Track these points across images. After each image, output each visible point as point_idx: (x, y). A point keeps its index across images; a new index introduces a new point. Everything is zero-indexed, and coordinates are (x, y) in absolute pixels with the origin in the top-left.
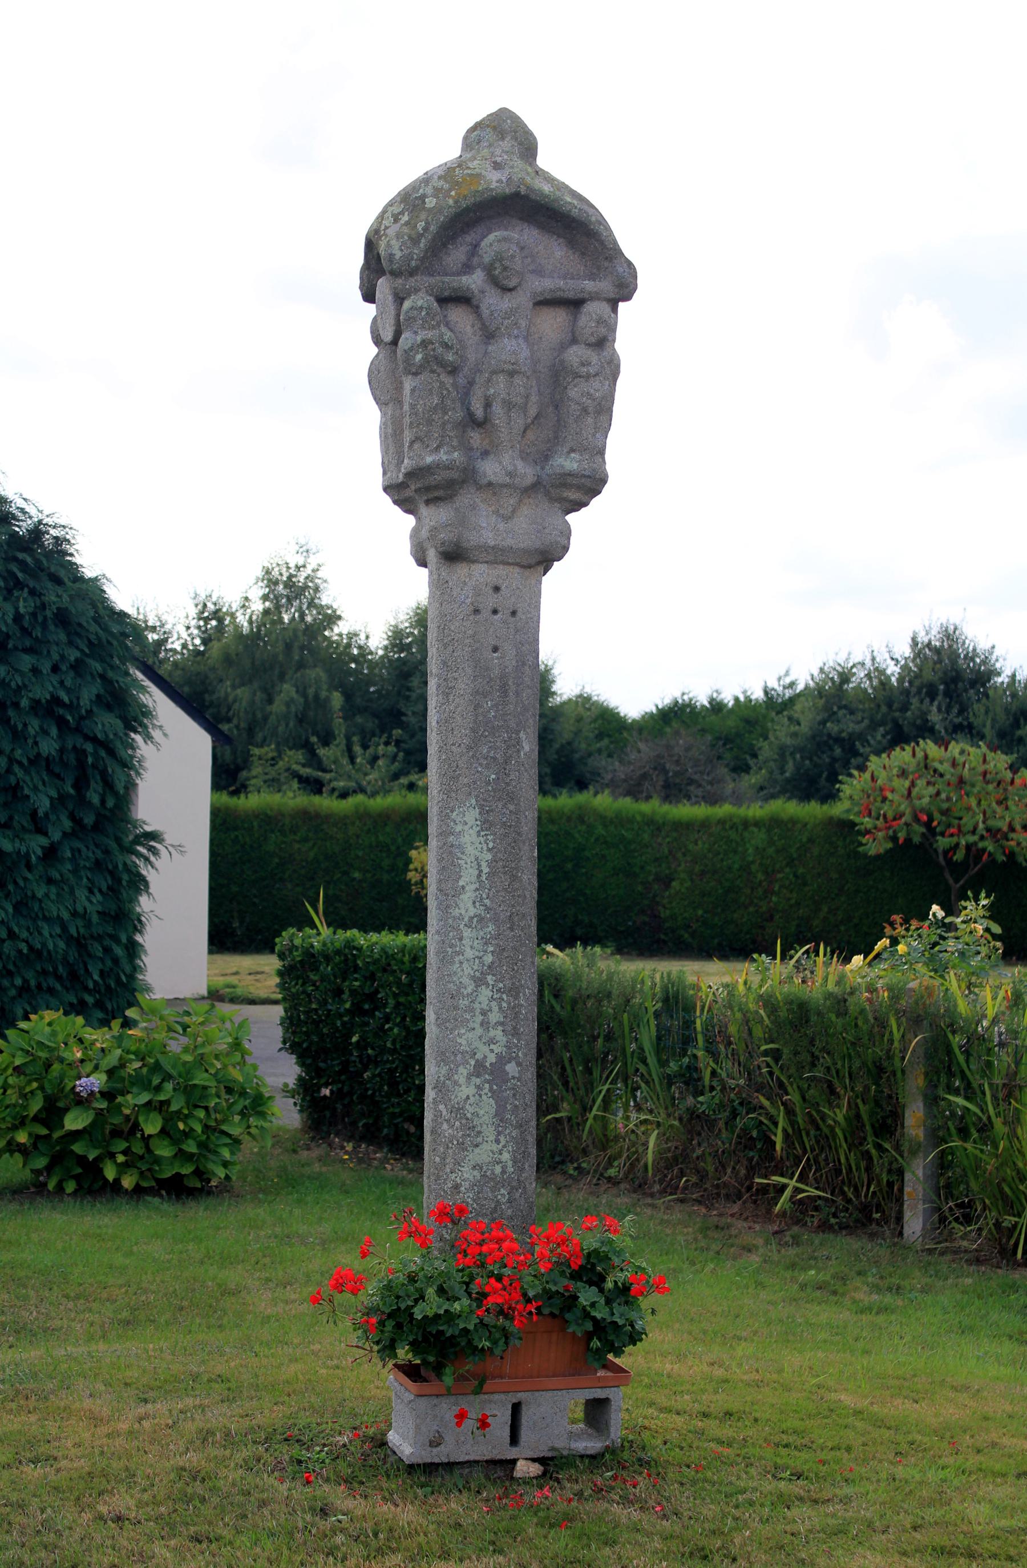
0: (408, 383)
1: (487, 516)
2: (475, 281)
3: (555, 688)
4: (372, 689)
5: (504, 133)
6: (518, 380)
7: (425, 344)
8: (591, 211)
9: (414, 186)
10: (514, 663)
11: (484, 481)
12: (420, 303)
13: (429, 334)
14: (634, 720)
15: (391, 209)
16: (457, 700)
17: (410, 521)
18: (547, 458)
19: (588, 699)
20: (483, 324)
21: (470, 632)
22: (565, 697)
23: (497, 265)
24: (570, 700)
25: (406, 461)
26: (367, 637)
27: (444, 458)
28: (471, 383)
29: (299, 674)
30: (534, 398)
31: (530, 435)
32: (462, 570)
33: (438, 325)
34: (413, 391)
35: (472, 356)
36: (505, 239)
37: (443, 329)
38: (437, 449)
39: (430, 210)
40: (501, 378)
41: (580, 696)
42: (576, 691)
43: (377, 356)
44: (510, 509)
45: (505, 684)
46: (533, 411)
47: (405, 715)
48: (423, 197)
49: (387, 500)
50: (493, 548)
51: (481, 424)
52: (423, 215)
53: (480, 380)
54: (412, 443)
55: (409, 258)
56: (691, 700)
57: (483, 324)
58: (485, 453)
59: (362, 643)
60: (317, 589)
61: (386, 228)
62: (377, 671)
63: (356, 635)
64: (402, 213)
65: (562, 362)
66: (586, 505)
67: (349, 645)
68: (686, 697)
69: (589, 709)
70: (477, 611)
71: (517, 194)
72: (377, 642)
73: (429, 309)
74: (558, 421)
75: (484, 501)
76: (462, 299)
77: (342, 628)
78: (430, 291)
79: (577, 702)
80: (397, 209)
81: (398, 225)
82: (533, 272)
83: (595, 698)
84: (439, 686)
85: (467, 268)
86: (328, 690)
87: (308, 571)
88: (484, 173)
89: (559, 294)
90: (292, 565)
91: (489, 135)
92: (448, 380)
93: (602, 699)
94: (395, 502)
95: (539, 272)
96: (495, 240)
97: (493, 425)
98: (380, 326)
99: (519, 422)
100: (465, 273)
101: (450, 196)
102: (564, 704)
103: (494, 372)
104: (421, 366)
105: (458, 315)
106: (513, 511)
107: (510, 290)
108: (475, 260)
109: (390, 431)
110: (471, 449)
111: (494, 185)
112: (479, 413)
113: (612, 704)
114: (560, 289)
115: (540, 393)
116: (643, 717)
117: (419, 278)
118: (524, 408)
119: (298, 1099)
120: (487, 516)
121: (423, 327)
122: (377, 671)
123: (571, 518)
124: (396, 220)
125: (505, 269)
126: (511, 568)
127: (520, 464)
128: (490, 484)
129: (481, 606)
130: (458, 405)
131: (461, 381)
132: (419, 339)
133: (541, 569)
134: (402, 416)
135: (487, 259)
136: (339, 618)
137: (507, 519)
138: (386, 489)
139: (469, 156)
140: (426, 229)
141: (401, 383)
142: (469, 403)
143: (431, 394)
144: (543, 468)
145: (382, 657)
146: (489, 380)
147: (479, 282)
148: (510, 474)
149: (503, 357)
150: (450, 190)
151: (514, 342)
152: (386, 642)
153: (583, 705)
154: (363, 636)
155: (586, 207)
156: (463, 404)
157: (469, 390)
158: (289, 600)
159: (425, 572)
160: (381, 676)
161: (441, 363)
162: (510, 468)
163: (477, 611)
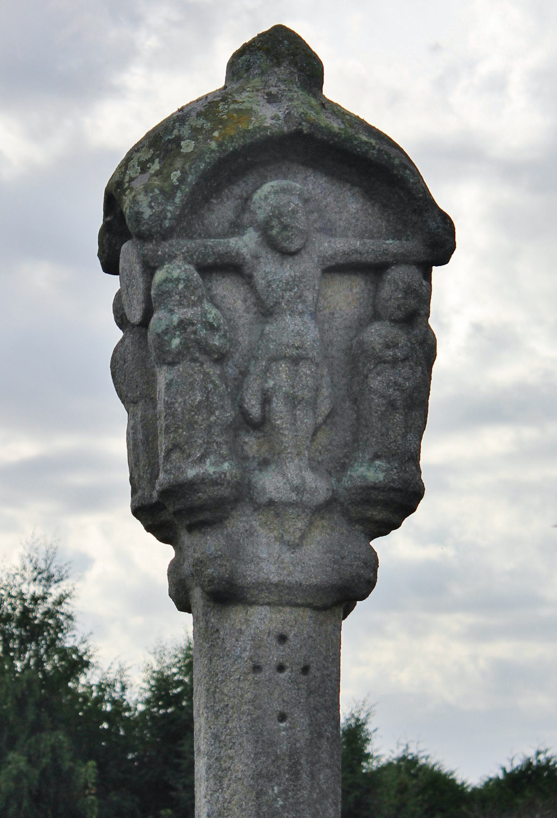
0: (163, 376)
1: (268, 545)
2: (246, 243)
3: (369, 749)
4: (130, 756)
5: (280, 57)
6: (305, 369)
7: (183, 325)
8: (393, 152)
9: (166, 126)
10: (307, 734)
11: (263, 500)
12: (176, 273)
13: (189, 313)
14: (475, 790)
15: (137, 156)
16: (234, 786)
17: (168, 552)
18: (344, 467)
19: (414, 762)
20: (258, 298)
21: (249, 696)
22: (384, 761)
23: (274, 223)
24: (390, 764)
25: (161, 476)
26: (124, 688)
27: (211, 470)
28: (244, 373)
29: (33, 739)
30: (325, 392)
31: (322, 438)
32: (237, 615)
33: (200, 300)
34: (169, 385)
35: (244, 339)
36: (284, 190)
37: (207, 306)
38: (202, 459)
39: (186, 156)
40: (283, 366)
41: (403, 758)
42: (398, 753)
43: (122, 341)
44: (298, 534)
45: (297, 763)
46: (324, 408)
47: (175, 789)
48: (178, 140)
49: (138, 526)
50: (276, 585)
51: (260, 425)
52: (178, 163)
53: (255, 369)
54: (169, 452)
55: (160, 217)
56: (548, 760)
57: (258, 298)
58: (264, 463)
59: (116, 696)
60: (59, 627)
61: (132, 179)
62: (136, 733)
63: (111, 686)
64: (151, 160)
65: (361, 343)
66: (397, 526)
67: (100, 700)
68: (542, 757)
69: (415, 776)
70: (257, 668)
71: (298, 133)
72: (137, 693)
73: (187, 280)
74: (358, 419)
75: (264, 524)
76: (231, 267)
77: (88, 679)
78: (189, 258)
79: (398, 767)
80: (144, 156)
81: (146, 176)
82: (320, 230)
83: (422, 761)
84: (209, 767)
85: (236, 228)
86: (73, 759)
87: (49, 603)
88: (255, 107)
89: (355, 257)
90: (28, 597)
91: (261, 60)
92: (214, 371)
93: (432, 762)
94: (149, 529)
95: (329, 230)
96: (270, 193)
97: (274, 427)
98: (126, 303)
99: (307, 421)
100: (233, 234)
101: (212, 138)
102: (382, 770)
103: (274, 359)
104: (179, 353)
105: (227, 290)
106: (302, 537)
107: (293, 254)
108: (247, 217)
109: (140, 436)
110: (246, 458)
111: (268, 123)
112: (255, 411)
113: (446, 768)
114: (356, 251)
115: (333, 385)
116: (487, 784)
117: (174, 241)
118: (313, 404)
119: (430, 766)
120: (268, 545)
121: (180, 304)
122: (136, 733)
123: (377, 544)
124: (144, 169)
125: (285, 227)
126: (300, 611)
127: (310, 477)
128: (271, 503)
129: (262, 661)
130: (228, 402)
131: (231, 371)
132: (175, 319)
133: (339, 611)
134: (155, 418)
135: (261, 215)
136: (87, 664)
137: (294, 547)
138: (137, 512)
139: (235, 86)
140: (182, 180)
141: (154, 375)
142: (242, 399)
143: (193, 389)
144: (339, 481)
145: (142, 714)
146: (267, 370)
147: (252, 245)
148: (296, 489)
149: (285, 340)
150: (213, 130)
151: (298, 320)
152: (148, 695)
153: (408, 770)
154: (118, 687)
155: (386, 147)
156: (234, 400)
157: (242, 382)
158: (23, 642)
159: (188, 618)
160: (142, 739)
161: (205, 349)
162: (296, 481)
163: (257, 668)
